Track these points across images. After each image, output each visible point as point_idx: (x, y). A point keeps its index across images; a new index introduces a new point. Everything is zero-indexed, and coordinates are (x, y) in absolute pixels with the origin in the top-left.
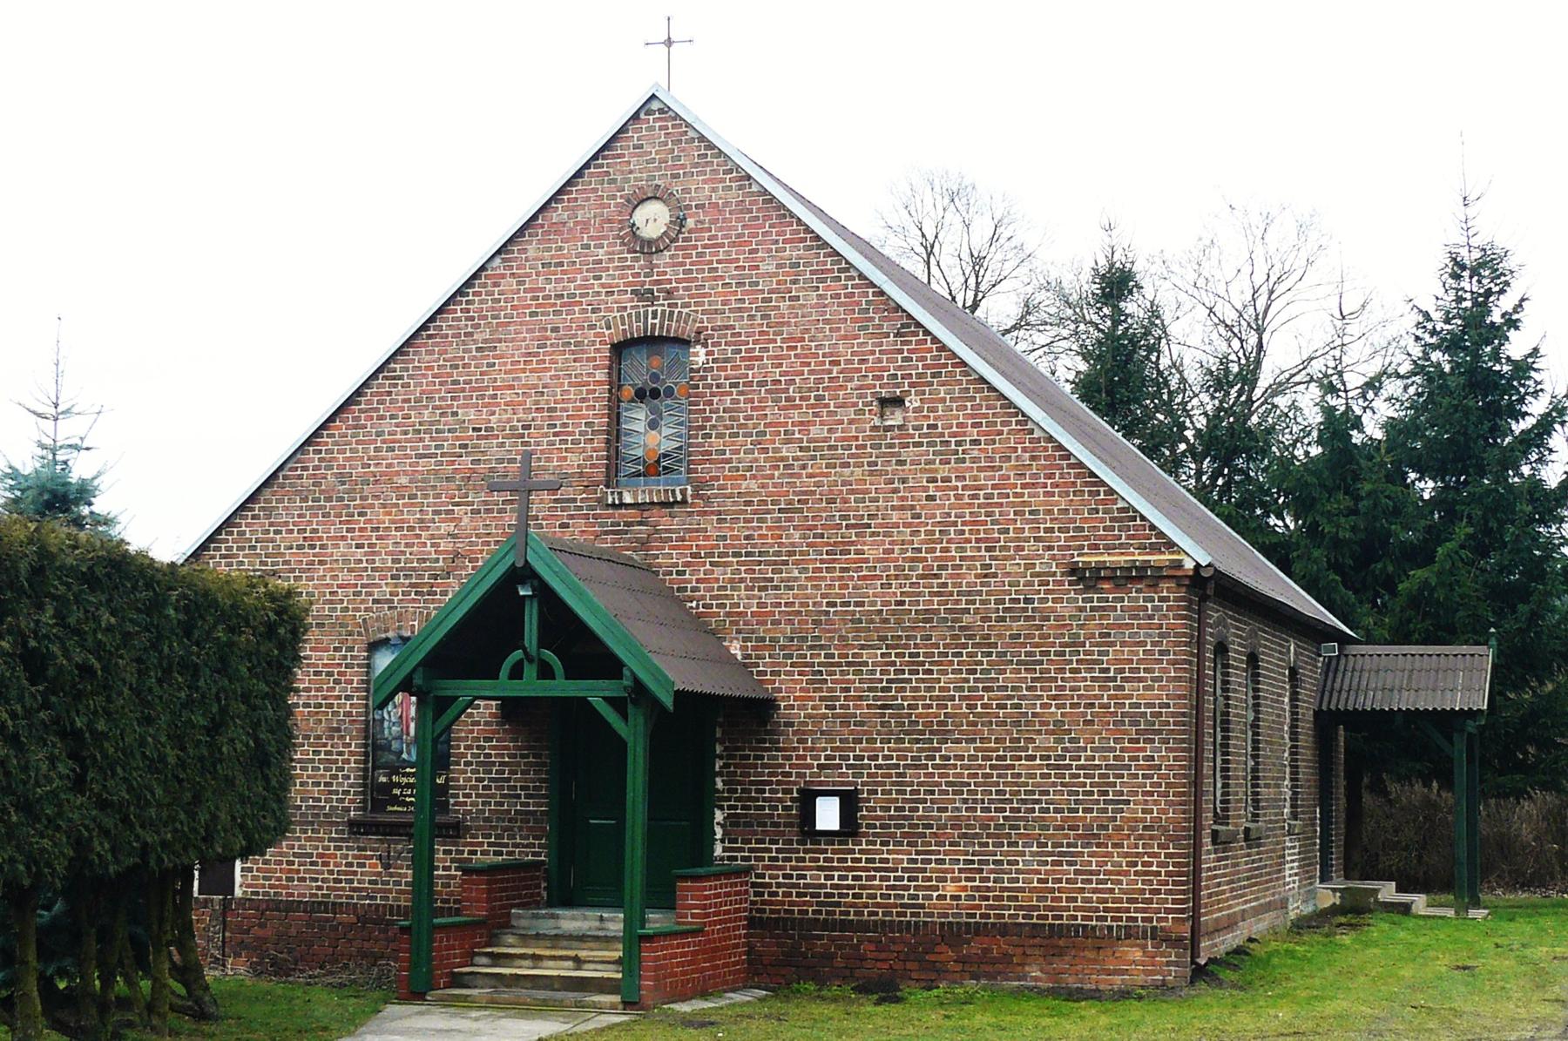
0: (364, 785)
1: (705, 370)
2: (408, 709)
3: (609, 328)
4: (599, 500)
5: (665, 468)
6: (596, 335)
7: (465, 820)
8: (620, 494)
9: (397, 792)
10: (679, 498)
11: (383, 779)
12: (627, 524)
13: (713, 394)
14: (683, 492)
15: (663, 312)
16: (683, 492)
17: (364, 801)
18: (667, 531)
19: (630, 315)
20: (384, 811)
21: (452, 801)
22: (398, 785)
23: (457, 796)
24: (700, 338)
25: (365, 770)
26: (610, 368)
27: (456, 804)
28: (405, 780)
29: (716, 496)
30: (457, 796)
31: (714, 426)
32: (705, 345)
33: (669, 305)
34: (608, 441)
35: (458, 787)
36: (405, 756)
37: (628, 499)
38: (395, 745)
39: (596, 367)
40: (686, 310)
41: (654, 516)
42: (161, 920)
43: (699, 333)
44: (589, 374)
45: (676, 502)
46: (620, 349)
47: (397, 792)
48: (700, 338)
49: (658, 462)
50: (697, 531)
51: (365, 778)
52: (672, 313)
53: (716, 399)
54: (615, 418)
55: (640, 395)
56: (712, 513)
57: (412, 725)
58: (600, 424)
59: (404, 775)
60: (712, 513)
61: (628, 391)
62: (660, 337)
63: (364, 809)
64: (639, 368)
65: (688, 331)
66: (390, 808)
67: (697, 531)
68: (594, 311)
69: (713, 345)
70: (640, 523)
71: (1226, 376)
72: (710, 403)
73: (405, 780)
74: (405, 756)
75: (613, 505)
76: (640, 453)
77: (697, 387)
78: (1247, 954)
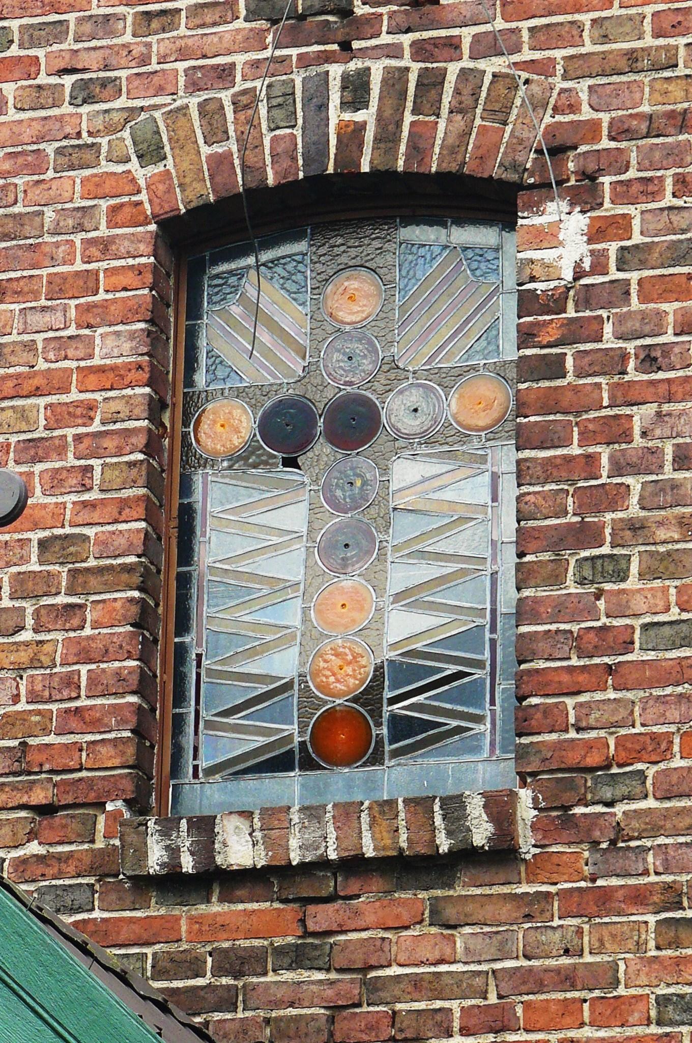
1: (587, 298)
3: (150, 153)
4: (103, 868)
5: (403, 727)
6: (95, 188)
8: (205, 827)
10: (481, 833)
12: (236, 963)
13: (627, 396)
14: (500, 808)
15: (395, 81)
16: (500, 808)
18: (418, 986)
19: (245, 103)
24: (565, 168)
26: (156, 320)
29: (654, 825)
31: (636, 527)
32: (585, 194)
33: (421, 51)
34: (143, 620)
37: (239, 849)
39: (91, 317)
40: (491, 66)
41: (363, 919)
43: (558, 151)
44: (61, 345)
45: (466, 857)
46: (201, 243)
48: (565, 168)
49: (370, 697)
50: (567, 979)
52: (431, 83)
53: (641, 416)
54: (173, 528)
55: (287, 432)
56: (638, 897)
58: (105, 548)
60: (638, 897)
61: (228, 424)
62: (383, 177)
65: (509, 144)
67: (567, 979)
68: (86, 94)
69: (623, 192)
70: (297, 957)
72: (615, 431)
75: (173, 884)
76: (284, 664)
77: (555, 367)
78: (655, 913)
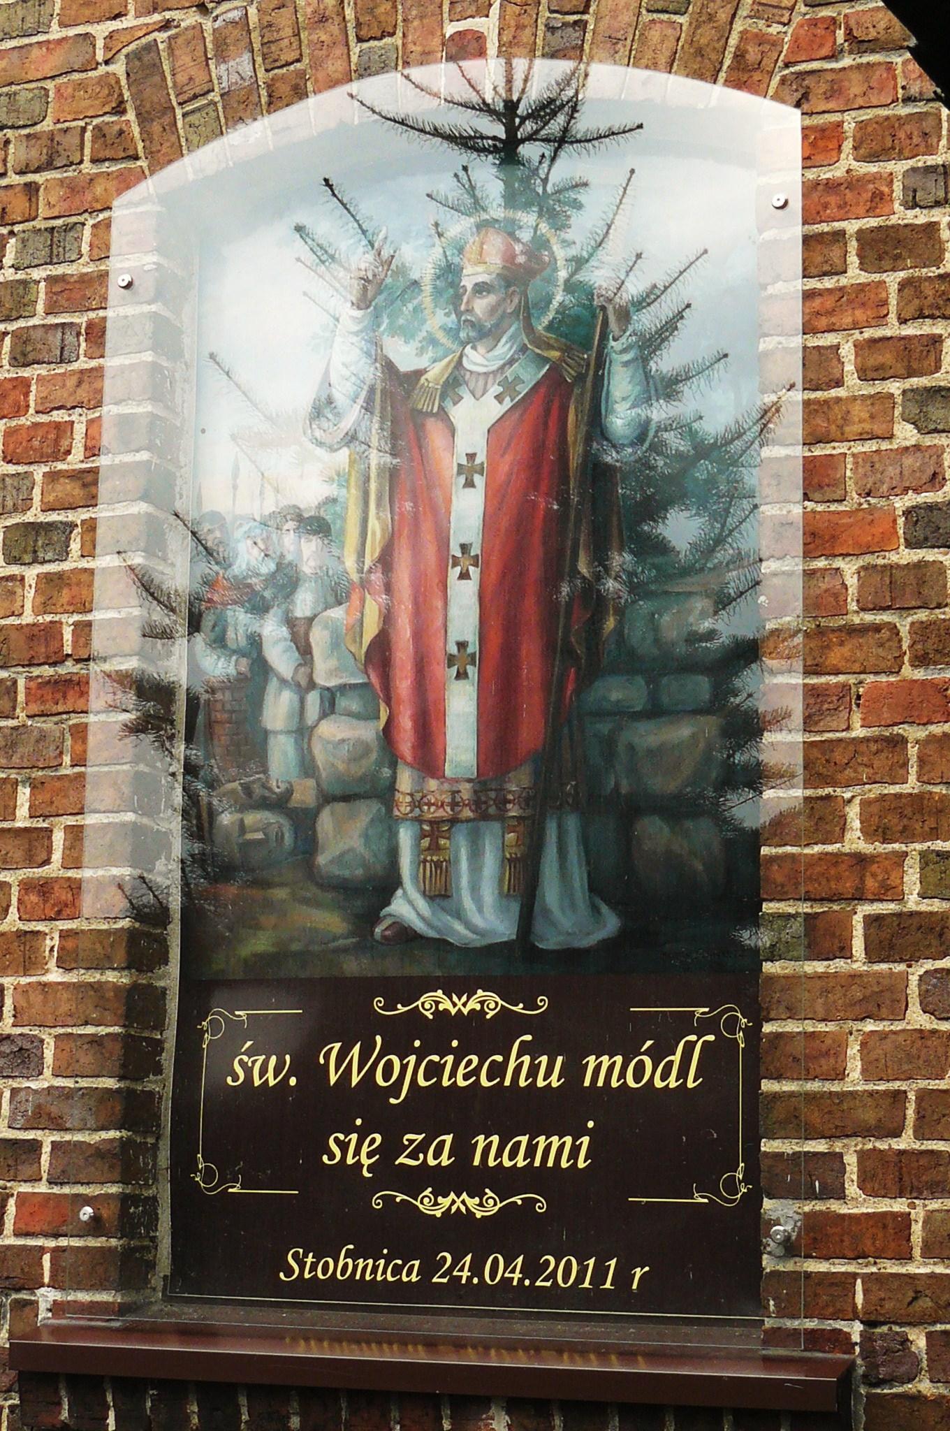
0: (132, 1110)
2: (429, 595)
7: (890, 1359)
9: (355, 1151)
11: (257, 1068)
17: (131, 1217)
20: (256, 1274)
21: (783, 1214)
22: (366, 1105)
23: (819, 1177)
25: (139, 1006)
27: (818, 1236)
28: (408, 1072)
30: (819, 1177)
35: (837, 1117)
36: (408, 907)
38: (343, 840)
42: (856, 326)
47: (355, 1151)
51: (135, 1057)
57: (461, 705)
59: (404, 1034)
63: (129, 1268)
64: (21, 360)
66: (301, 1265)
71: (823, 1308)
73: (408, 1072)
74: (408, 907)
